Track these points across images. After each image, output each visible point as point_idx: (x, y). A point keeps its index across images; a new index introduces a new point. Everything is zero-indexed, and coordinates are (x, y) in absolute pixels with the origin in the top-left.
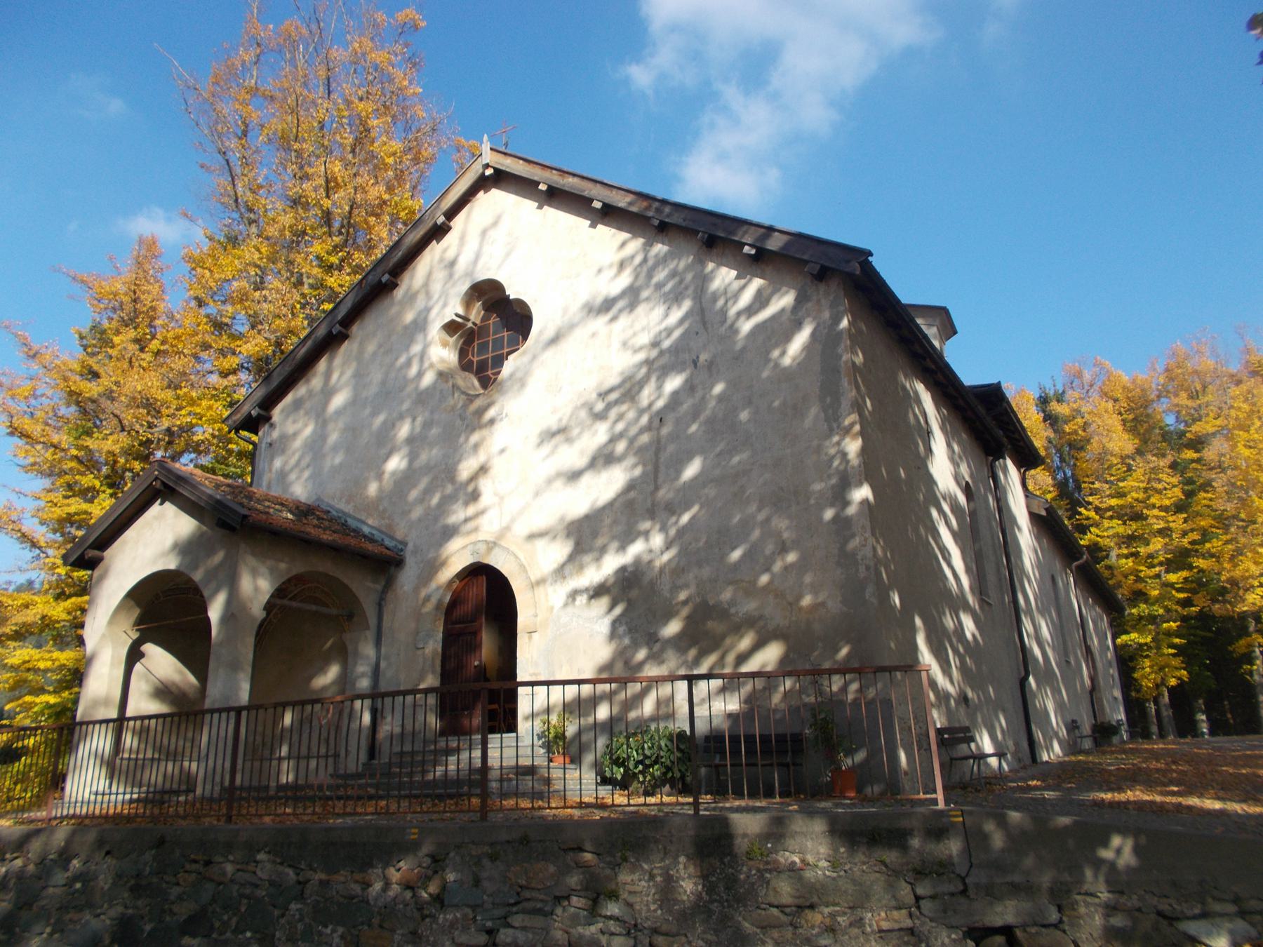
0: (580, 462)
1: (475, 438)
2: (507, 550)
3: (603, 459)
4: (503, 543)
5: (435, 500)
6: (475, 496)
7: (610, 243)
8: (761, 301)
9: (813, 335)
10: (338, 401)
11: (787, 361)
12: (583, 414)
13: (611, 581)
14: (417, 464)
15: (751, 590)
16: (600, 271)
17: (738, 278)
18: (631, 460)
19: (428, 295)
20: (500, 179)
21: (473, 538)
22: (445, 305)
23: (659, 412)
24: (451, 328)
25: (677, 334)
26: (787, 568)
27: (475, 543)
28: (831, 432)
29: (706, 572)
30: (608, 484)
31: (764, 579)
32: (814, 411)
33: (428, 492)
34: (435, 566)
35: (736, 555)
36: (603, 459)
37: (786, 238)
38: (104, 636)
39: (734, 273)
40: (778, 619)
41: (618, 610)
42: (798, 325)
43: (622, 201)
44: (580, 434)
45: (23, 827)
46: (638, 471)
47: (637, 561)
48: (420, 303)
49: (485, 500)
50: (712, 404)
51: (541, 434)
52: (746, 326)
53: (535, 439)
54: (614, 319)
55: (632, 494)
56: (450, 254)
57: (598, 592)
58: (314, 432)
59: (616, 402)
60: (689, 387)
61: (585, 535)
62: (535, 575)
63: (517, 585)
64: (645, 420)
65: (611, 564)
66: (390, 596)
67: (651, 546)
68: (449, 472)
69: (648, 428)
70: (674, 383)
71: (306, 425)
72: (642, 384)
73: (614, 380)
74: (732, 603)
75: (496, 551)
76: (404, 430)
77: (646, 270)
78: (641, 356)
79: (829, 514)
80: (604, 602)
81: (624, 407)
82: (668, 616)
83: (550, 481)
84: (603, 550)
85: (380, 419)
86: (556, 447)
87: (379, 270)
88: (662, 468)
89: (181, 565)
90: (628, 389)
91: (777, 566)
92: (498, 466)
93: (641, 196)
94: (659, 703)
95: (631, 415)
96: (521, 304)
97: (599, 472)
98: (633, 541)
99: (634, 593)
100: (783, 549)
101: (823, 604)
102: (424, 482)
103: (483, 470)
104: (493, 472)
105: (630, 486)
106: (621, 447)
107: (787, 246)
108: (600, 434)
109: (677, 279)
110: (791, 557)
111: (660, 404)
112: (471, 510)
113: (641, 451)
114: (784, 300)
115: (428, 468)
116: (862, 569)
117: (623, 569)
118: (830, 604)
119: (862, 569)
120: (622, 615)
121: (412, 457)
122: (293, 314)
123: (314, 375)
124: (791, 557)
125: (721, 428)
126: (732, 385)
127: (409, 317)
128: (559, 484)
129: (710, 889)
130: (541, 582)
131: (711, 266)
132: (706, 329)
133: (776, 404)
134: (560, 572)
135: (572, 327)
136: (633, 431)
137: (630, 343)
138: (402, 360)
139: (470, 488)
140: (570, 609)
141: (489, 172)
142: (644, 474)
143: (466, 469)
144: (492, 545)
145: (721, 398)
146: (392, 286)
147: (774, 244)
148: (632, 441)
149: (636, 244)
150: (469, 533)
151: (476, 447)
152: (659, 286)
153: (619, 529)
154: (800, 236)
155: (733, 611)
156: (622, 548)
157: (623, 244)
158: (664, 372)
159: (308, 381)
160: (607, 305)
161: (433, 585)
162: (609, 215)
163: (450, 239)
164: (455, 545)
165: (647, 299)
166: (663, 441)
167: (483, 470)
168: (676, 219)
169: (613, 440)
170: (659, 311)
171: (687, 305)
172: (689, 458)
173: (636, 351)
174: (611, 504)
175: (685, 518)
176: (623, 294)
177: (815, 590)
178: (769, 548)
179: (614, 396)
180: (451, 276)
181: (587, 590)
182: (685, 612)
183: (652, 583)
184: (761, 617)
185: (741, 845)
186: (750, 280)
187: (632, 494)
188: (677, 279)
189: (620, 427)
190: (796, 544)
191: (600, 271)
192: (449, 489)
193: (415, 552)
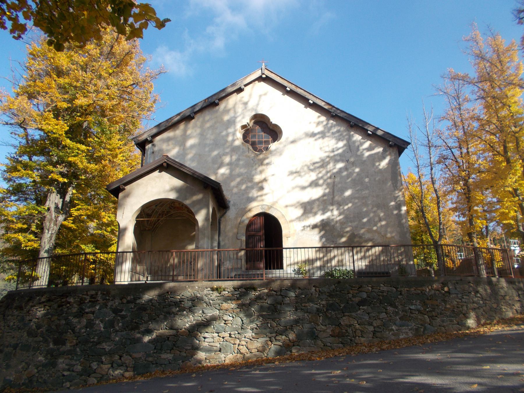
0: (307, 184)
1: (261, 168)
2: (275, 209)
3: (314, 184)
4: (274, 207)
5: (244, 187)
6: (262, 188)
7: (313, 115)
8: (369, 149)
9: (389, 161)
10: (190, 142)
11: (381, 167)
12: (306, 168)
13: (319, 224)
14: (234, 173)
15: (370, 231)
16: (310, 123)
17: (362, 139)
18: (325, 187)
19: (235, 112)
20: (267, 80)
21: (261, 203)
22: (243, 118)
23: (334, 174)
24: (243, 127)
25: (340, 151)
26: (381, 226)
27: (262, 205)
28: (395, 190)
29: (355, 224)
30: (317, 193)
31: (375, 228)
32: (389, 183)
33: (239, 184)
34: (245, 211)
35: (365, 220)
36: (314, 184)
37: (382, 133)
38: (130, 221)
39: (361, 137)
40: (380, 240)
41: (322, 233)
42: (384, 158)
43: (322, 104)
44: (305, 174)
45: (242, 282)
46: (327, 191)
47: (328, 219)
48: (232, 114)
49: (265, 192)
50: (355, 175)
51: (290, 172)
52: (367, 154)
53: (288, 174)
54: (316, 140)
55: (325, 198)
56: (245, 100)
57: (314, 227)
58: (178, 152)
59: (318, 167)
60: (346, 168)
61: (308, 208)
62: (288, 219)
63: (281, 221)
64: (329, 175)
65: (318, 218)
66: (223, 219)
67: (334, 214)
68: (250, 179)
69: (330, 177)
70: (340, 165)
71: (173, 148)
72: (328, 163)
73: (317, 160)
74: (363, 234)
75: (272, 209)
76: (227, 159)
77: (328, 129)
78: (327, 154)
79: (395, 212)
80: (316, 230)
81: (321, 169)
82: (342, 236)
83: (294, 188)
84: (315, 214)
85: (215, 153)
86: (295, 177)
87: (215, 98)
88: (335, 191)
89: (177, 198)
90: (323, 164)
91: (379, 225)
92: (270, 179)
93: (328, 104)
94: (338, 261)
95: (324, 172)
96: (276, 126)
97: (313, 188)
98: (326, 212)
99: (328, 228)
100: (380, 220)
101: (393, 237)
102: (238, 180)
103: (265, 180)
104: (269, 182)
105: (324, 195)
106: (321, 182)
107: (383, 134)
108: (313, 176)
109: (339, 134)
110: (383, 223)
111: (335, 171)
112: (260, 193)
113: (328, 185)
114: (380, 150)
115: (239, 175)
116: (405, 229)
117: (323, 220)
118: (396, 237)
119: (405, 229)
120: (323, 235)
121: (231, 170)
122: (508, 161)
123: (178, 128)
124: (383, 223)
125: (358, 183)
126: (361, 170)
127: (226, 118)
128: (297, 189)
129: (492, 291)
130: (291, 221)
131: (352, 133)
132: (351, 152)
133: (377, 179)
134: (299, 219)
135: (300, 139)
136: (325, 177)
137: (323, 149)
138: (224, 133)
139: (260, 185)
140: (304, 232)
141: (264, 76)
142: (329, 192)
143: (258, 178)
144: (270, 207)
145: (358, 174)
146: (217, 104)
147: (379, 133)
148: (325, 181)
149: (323, 118)
150: (260, 201)
151: (261, 172)
152: (333, 133)
153: (321, 207)
154: (388, 133)
155: (363, 236)
156: (323, 213)
157: (319, 117)
158: (336, 161)
159: (175, 131)
160: (313, 135)
161: (244, 218)
162: (315, 106)
163: (242, 94)
164: (254, 204)
165: (328, 137)
166: (336, 183)
167: (265, 180)
168: (341, 115)
169: (318, 179)
170: (333, 141)
171: (345, 142)
172: (346, 189)
173: (326, 152)
174: (318, 199)
175: (346, 207)
176: (319, 133)
177: (391, 233)
178: (377, 219)
179: (317, 165)
180: (246, 108)
181: (309, 226)
182: (348, 235)
183: (333, 226)
184: (373, 239)
185: (494, 283)
186: (366, 141)
187: (325, 198)
188: (339, 134)
189: (320, 175)
190: (385, 219)
191: (310, 123)
192: (250, 184)
193: (234, 205)
